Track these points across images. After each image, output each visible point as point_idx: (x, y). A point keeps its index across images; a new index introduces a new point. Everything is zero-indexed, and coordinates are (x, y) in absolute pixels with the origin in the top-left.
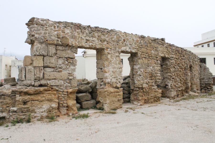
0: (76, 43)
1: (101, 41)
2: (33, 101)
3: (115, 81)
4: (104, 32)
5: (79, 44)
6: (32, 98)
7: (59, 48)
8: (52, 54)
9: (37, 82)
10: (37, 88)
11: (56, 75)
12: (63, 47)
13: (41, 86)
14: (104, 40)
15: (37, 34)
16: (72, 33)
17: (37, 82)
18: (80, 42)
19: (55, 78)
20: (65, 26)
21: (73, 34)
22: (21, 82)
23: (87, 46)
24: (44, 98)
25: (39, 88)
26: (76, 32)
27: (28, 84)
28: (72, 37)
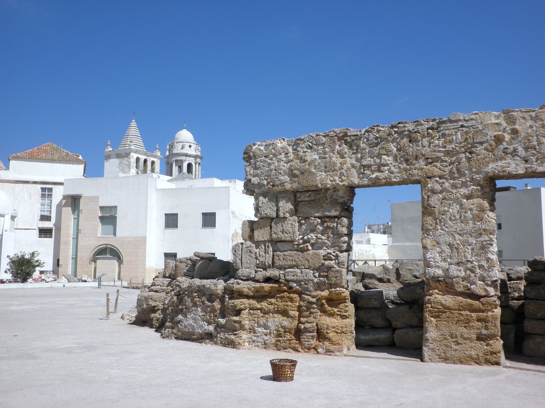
0: (334, 180)
1: (407, 161)
2: (253, 310)
3: (463, 274)
4: (415, 132)
5: (342, 181)
6: (250, 304)
7: (302, 198)
8: (284, 214)
9: (261, 271)
10: (258, 285)
11: (296, 257)
12: (310, 193)
13: (268, 280)
14: (416, 156)
15: (254, 176)
16: (325, 158)
17: (261, 271)
18: (345, 176)
19: (294, 263)
20: (309, 145)
21: (328, 159)
22: (511, 288)
23: (521, 172)
24: (271, 307)
25: (264, 285)
26: (334, 153)
27: (244, 276)
28: (325, 168)
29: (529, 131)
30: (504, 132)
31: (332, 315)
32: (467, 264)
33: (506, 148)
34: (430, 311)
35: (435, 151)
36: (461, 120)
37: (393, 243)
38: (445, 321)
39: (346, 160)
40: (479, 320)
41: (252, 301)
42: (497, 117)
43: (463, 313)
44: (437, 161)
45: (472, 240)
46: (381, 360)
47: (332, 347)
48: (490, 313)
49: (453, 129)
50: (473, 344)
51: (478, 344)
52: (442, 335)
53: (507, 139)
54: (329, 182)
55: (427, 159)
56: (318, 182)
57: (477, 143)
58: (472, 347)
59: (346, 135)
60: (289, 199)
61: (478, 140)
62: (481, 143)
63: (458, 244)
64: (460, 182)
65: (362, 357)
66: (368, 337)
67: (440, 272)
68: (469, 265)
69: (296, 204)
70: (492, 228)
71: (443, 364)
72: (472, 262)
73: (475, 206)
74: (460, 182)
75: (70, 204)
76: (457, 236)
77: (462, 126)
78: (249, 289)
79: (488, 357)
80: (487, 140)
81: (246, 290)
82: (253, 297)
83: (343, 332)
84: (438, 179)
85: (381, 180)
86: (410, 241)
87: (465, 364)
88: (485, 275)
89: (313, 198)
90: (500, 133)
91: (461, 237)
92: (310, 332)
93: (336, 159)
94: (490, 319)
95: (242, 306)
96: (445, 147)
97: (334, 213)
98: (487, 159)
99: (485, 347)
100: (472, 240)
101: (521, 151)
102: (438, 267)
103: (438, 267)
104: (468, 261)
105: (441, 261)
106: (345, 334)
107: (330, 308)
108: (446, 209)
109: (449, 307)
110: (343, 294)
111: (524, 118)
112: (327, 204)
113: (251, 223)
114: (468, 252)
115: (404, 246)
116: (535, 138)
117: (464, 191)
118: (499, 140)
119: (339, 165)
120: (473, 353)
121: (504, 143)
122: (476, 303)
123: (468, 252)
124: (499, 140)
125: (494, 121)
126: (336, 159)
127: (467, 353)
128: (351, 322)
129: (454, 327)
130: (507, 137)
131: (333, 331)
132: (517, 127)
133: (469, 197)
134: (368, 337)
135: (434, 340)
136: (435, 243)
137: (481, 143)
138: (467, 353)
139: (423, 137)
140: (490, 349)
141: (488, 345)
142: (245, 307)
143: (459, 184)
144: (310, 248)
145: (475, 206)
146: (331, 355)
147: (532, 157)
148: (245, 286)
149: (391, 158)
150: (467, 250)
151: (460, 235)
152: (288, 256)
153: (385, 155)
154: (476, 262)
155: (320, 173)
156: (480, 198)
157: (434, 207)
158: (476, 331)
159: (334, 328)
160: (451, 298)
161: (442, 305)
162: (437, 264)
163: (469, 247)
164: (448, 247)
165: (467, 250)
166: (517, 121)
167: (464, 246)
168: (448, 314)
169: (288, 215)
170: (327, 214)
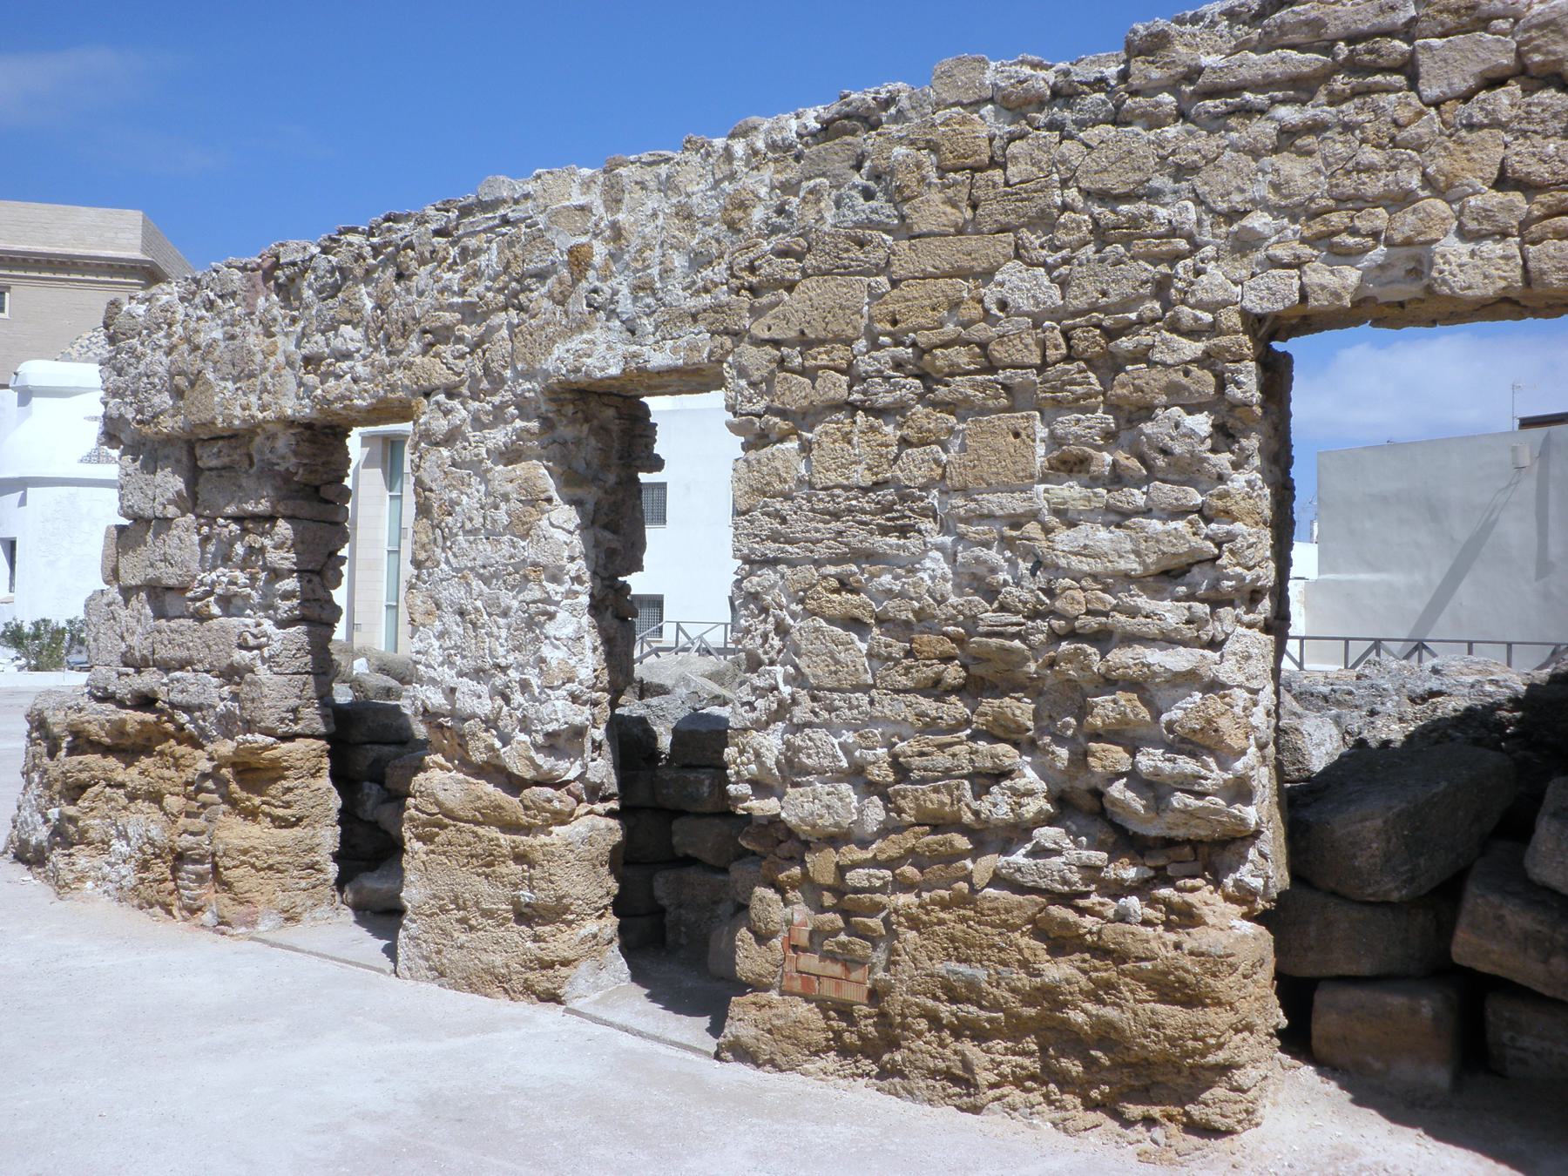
5: (263, 408)
12: (220, 443)
29: (647, 230)
30: (596, 235)
31: (251, 814)
32: (493, 676)
33: (595, 291)
34: (412, 819)
35: (441, 308)
36: (504, 201)
37: (1320, 572)
38: (444, 853)
39: (275, 343)
40: (520, 858)
41: (111, 762)
42: (587, 185)
43: (481, 831)
44: (446, 341)
45: (510, 600)
46: (315, 960)
47: (233, 911)
48: (542, 838)
49: (484, 231)
50: (500, 932)
51: (517, 934)
52: (435, 896)
53: (597, 260)
54: (238, 411)
55: (425, 332)
56: (218, 409)
57: (531, 276)
58: (497, 943)
59: (277, 265)
60: (178, 461)
61: (532, 266)
62: (541, 276)
63: (477, 609)
64: (489, 407)
65: (281, 946)
66: (386, 886)
67: (436, 699)
68: (500, 679)
69: (193, 475)
70: (551, 559)
71: (434, 987)
72: (504, 669)
73: (515, 484)
74: (489, 407)
75: (379, 458)
76: (477, 584)
77: (505, 221)
78: (102, 727)
79: (530, 975)
80: (553, 263)
81: (93, 729)
82: (106, 751)
83: (270, 867)
84: (441, 397)
85: (332, 403)
86: (1372, 567)
87: (476, 991)
88: (531, 713)
89: (226, 460)
90: (584, 239)
91: (485, 589)
92: (195, 862)
93: (254, 340)
94: (538, 856)
95: (84, 776)
96: (462, 292)
97: (263, 506)
98: (550, 330)
99: (529, 944)
100: (510, 600)
101: (625, 305)
102: (433, 682)
103: (433, 682)
104: (498, 666)
105: (442, 664)
106: (279, 871)
107: (244, 795)
108: (454, 495)
109: (452, 810)
110: (267, 754)
111: (642, 185)
112: (249, 476)
113: (121, 529)
114: (498, 638)
115: (1352, 582)
116: (658, 251)
117: (499, 437)
118: (578, 261)
119: (259, 357)
120: (498, 960)
121: (591, 273)
122: (511, 802)
123: (498, 638)
124: (578, 261)
125: (578, 199)
126: (254, 340)
127: (484, 957)
128: (329, 837)
129: (462, 875)
130: (600, 251)
131: (243, 863)
132: (621, 217)
133: (510, 455)
134: (386, 886)
135: (418, 910)
136: (431, 606)
137: (541, 276)
138: (484, 957)
139: (422, 262)
140: (538, 952)
141: (537, 939)
142: (93, 777)
143: (487, 413)
144: (215, 610)
145: (515, 484)
146: (223, 934)
147: (645, 321)
148: (91, 718)
149: (358, 334)
150: (495, 629)
151: (486, 581)
152: (180, 635)
153: (347, 322)
154: (517, 669)
155: (222, 384)
156: (539, 458)
157: (431, 490)
158: (508, 891)
159: (245, 852)
160: (459, 782)
161: (438, 804)
162: (433, 673)
163: (502, 621)
164: (458, 618)
165: (495, 629)
166: (627, 196)
167: (490, 615)
168: (449, 833)
169: (171, 511)
170: (250, 507)
